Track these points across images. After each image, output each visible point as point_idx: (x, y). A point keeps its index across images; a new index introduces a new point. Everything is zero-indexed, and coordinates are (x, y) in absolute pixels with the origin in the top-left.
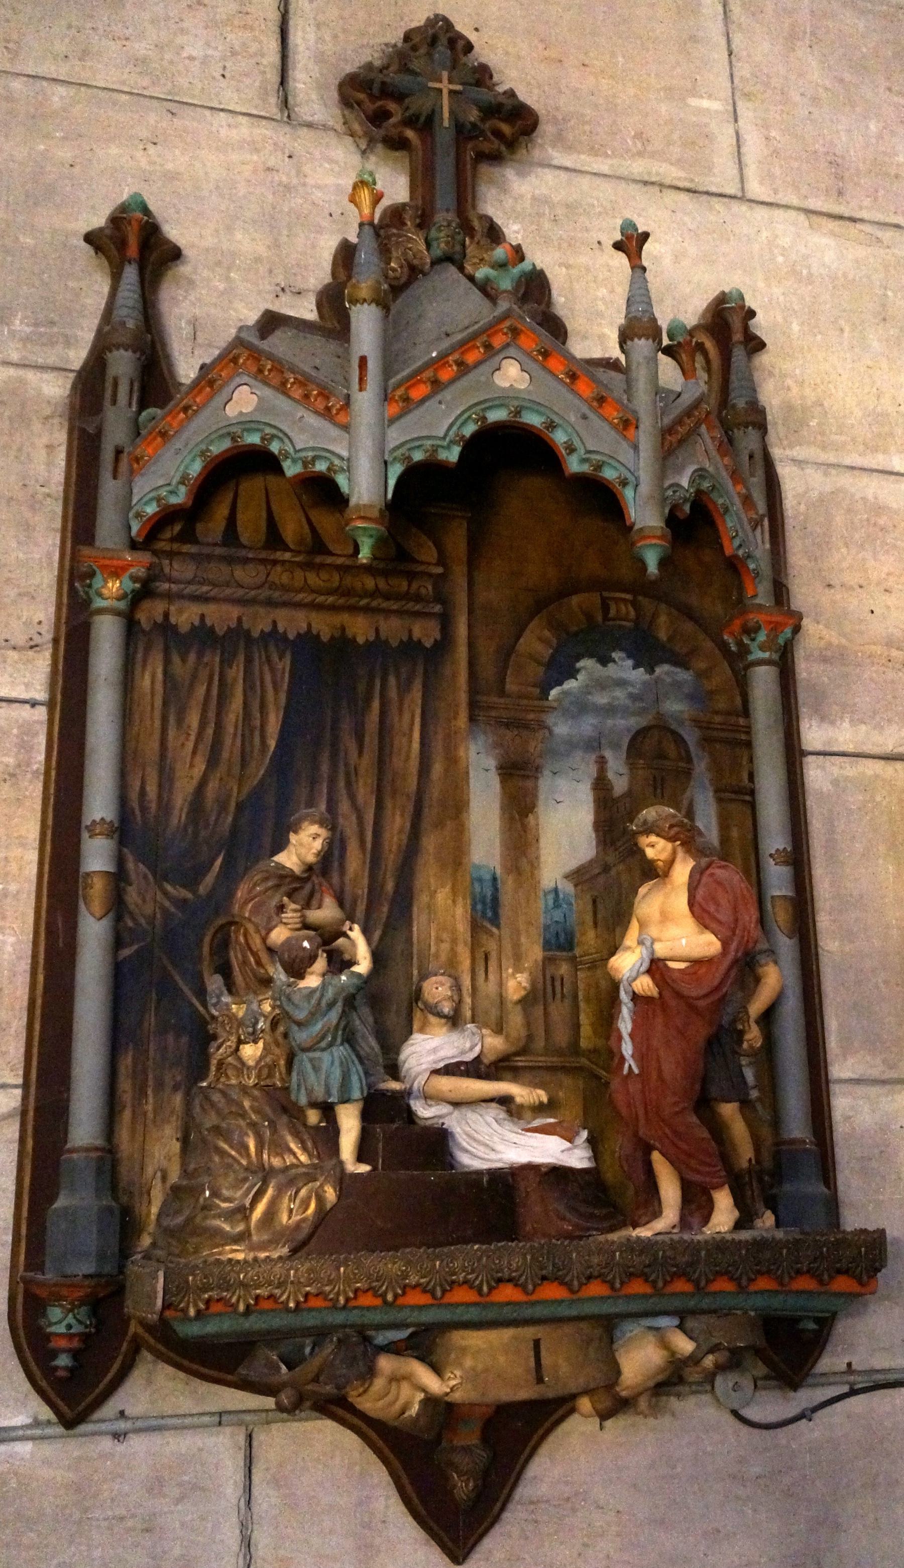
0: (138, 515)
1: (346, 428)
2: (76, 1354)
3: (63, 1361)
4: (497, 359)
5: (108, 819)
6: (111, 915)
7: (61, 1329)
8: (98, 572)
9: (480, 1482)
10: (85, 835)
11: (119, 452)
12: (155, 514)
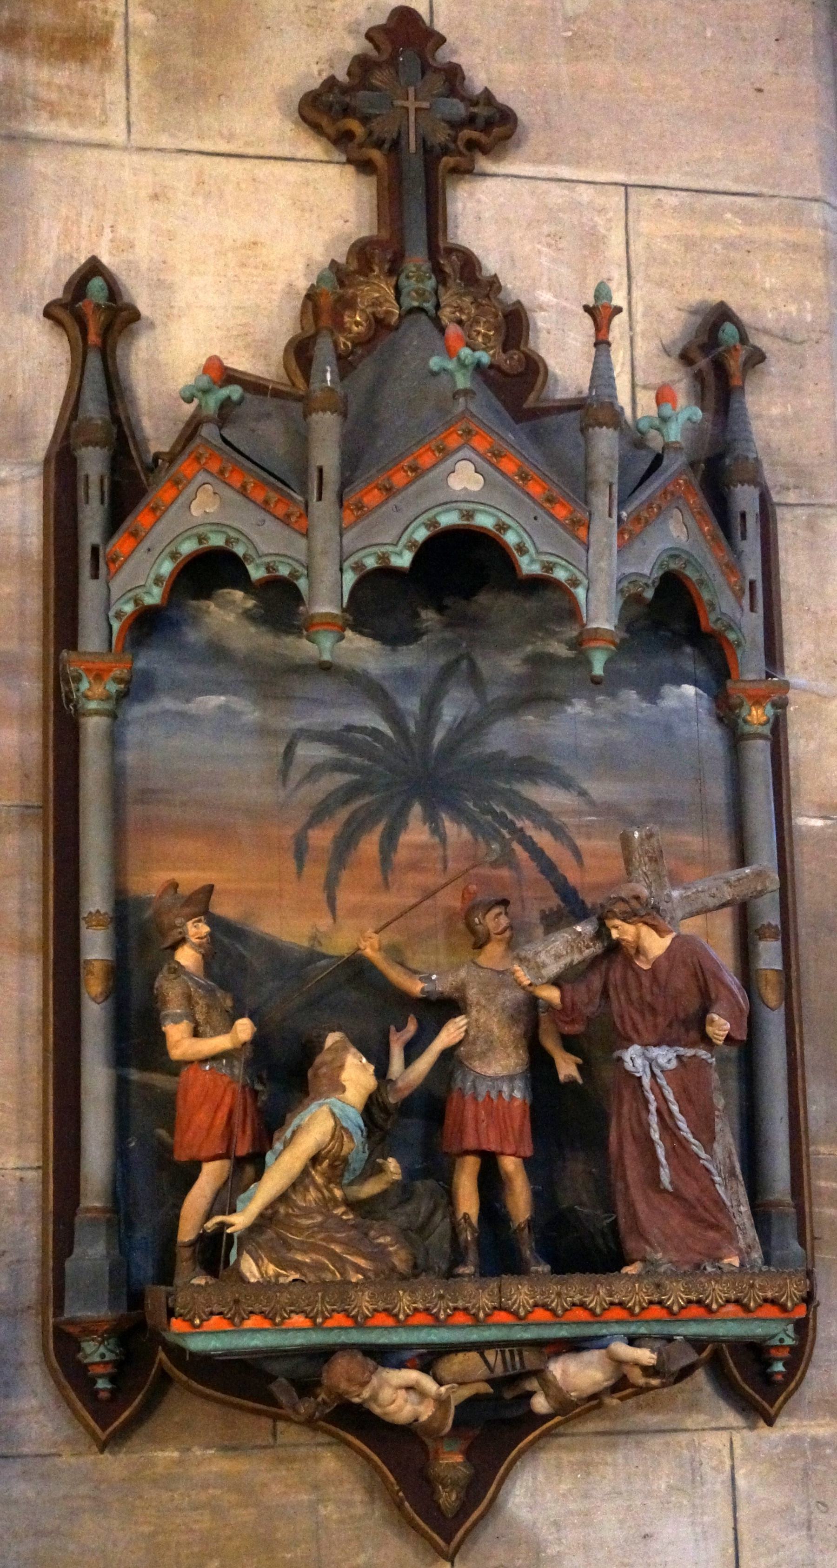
0: (119, 615)
1: (306, 535)
2: (112, 1379)
3: (102, 1384)
4: (449, 462)
5: (102, 911)
6: (110, 1000)
7: (97, 1359)
8: (84, 675)
9: (462, 1495)
10: (83, 924)
11: (95, 550)
12: (134, 612)
